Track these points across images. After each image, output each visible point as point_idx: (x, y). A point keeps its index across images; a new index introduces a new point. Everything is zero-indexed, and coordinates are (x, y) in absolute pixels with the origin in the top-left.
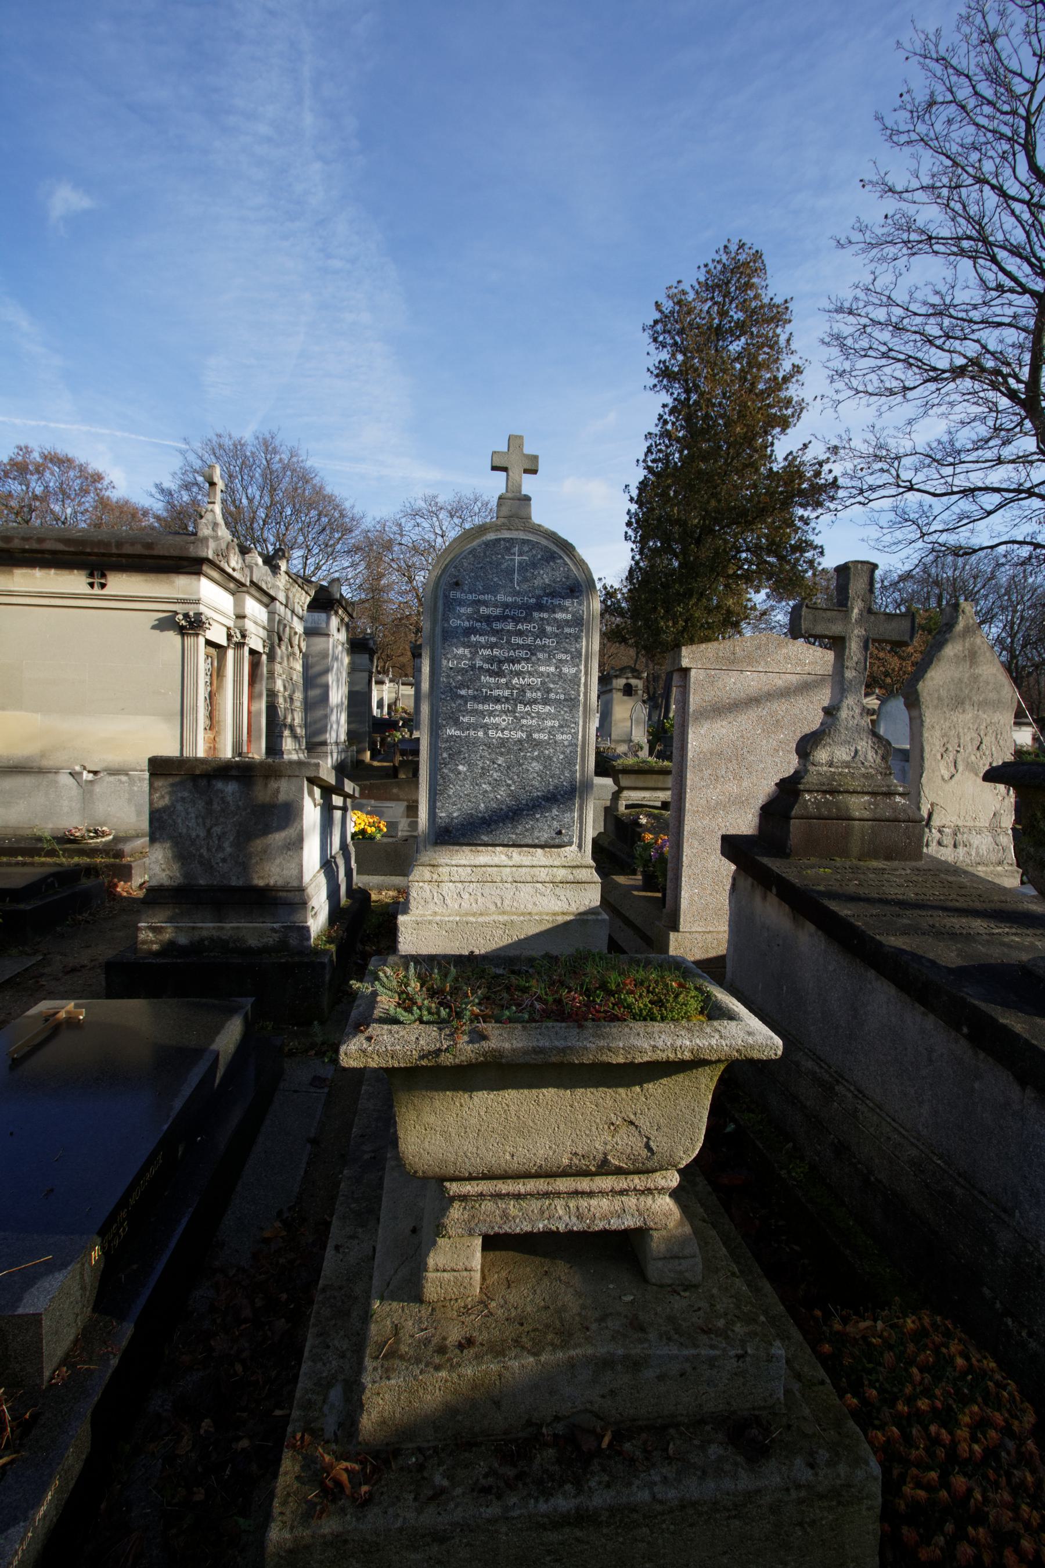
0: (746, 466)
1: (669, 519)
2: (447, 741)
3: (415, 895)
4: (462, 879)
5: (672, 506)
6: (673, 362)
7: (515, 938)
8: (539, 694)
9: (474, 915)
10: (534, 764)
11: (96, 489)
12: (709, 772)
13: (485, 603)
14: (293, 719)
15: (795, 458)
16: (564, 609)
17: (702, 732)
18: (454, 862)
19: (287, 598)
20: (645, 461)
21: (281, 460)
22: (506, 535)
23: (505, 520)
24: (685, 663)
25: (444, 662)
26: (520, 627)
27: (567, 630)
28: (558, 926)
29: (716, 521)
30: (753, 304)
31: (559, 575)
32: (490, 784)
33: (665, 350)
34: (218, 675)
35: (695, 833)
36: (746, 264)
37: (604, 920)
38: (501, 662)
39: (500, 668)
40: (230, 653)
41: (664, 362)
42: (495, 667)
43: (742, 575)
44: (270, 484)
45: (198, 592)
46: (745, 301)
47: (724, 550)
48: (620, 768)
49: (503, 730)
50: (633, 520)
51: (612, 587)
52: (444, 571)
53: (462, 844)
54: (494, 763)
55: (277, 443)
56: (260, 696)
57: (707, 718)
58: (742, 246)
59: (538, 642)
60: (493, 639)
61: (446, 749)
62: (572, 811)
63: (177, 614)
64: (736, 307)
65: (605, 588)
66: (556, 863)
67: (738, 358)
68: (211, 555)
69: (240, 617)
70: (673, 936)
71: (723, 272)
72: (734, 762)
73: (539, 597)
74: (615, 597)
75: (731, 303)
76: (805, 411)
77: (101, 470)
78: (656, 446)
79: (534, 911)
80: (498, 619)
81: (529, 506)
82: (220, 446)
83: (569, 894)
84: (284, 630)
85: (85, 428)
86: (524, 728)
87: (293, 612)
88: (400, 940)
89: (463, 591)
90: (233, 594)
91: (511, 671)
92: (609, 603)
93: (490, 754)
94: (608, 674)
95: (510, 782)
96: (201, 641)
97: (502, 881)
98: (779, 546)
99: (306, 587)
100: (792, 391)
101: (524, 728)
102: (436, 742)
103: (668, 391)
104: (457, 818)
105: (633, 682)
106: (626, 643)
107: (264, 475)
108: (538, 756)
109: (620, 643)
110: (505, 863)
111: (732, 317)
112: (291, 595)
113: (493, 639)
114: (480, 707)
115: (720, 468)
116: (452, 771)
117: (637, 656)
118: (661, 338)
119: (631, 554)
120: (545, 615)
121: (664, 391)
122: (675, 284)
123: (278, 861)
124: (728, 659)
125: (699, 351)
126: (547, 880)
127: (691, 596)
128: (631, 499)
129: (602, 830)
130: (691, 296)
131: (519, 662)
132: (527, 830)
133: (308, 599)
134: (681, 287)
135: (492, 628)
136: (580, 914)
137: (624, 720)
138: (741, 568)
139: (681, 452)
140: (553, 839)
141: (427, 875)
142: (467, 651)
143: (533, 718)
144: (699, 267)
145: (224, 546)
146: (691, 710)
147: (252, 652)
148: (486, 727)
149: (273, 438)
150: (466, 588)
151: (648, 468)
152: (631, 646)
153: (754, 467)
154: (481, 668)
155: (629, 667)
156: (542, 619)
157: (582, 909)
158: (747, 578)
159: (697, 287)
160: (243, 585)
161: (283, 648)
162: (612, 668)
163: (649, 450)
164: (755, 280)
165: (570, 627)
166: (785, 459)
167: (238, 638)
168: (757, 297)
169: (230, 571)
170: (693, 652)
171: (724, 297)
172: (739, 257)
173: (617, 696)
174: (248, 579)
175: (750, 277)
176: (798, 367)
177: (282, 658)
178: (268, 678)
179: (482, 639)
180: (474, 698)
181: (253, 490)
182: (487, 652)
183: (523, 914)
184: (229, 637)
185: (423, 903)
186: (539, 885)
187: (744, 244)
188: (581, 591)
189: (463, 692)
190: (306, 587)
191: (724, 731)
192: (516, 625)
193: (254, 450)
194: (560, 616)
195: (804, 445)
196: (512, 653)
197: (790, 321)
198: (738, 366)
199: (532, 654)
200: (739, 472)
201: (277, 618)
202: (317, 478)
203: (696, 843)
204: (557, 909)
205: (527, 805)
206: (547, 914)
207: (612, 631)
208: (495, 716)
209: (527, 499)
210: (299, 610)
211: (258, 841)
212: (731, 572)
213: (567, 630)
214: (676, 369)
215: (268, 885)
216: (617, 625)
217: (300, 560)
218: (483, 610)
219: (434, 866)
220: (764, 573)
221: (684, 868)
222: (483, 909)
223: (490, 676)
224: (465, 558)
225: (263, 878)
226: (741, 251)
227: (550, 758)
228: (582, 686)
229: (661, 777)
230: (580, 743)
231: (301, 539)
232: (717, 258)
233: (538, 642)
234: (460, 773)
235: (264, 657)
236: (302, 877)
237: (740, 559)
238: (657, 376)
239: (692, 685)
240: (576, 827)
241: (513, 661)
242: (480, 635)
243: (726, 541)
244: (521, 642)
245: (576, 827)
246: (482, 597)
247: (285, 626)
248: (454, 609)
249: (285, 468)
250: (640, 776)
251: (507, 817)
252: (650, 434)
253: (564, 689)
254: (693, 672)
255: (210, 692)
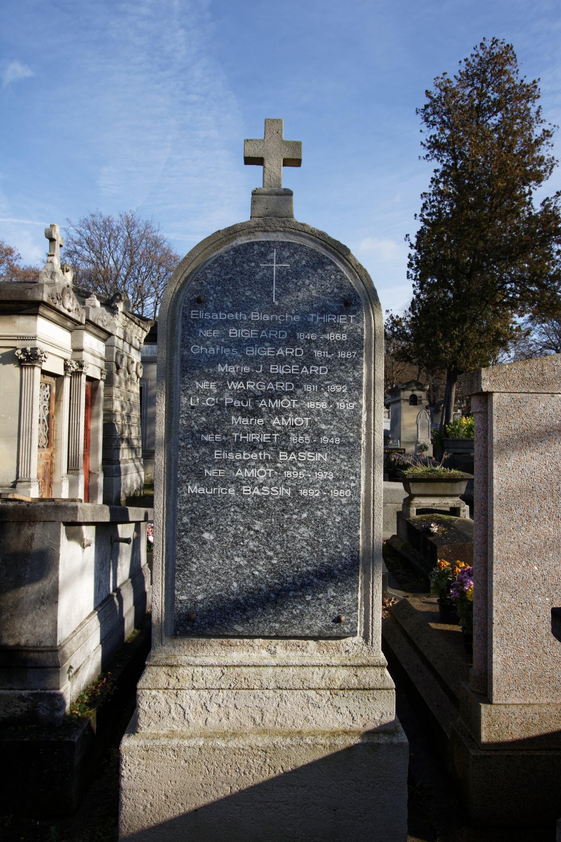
0: (508, 212)
1: (444, 260)
2: (188, 502)
3: (146, 708)
4: (209, 685)
5: (447, 248)
6: (442, 136)
7: (280, 770)
8: (307, 438)
9: (224, 736)
10: (303, 529)
11: (8, 260)
12: (520, 511)
13: (235, 323)
14: (130, 433)
15: (549, 205)
16: (337, 328)
17: (509, 465)
18: (198, 661)
19: (125, 333)
20: (421, 215)
21: (139, 232)
22: (261, 237)
23: (260, 220)
24: (486, 386)
25: (184, 400)
26: (280, 352)
27: (342, 354)
28: (338, 753)
29: (485, 259)
30: (507, 86)
31: (329, 285)
32: (245, 556)
33: (435, 127)
34: (56, 400)
35: (506, 584)
36: (499, 56)
37: (401, 744)
38: (256, 398)
39: (255, 406)
40: (67, 381)
41: (435, 136)
42: (249, 405)
43: (507, 302)
44: (130, 251)
45: (35, 330)
46: (499, 84)
47: (492, 282)
48: (411, 477)
49: (260, 486)
50: (414, 262)
51: (397, 317)
52: (183, 286)
53: (209, 636)
54: (249, 529)
55: (136, 219)
56: (98, 416)
57: (514, 449)
58: (495, 42)
59: (304, 370)
60: (247, 369)
61: (186, 512)
62: (354, 590)
63: (16, 349)
64: (493, 89)
65: (392, 318)
66: (334, 661)
67: (496, 129)
68: (45, 299)
69: (78, 350)
70: (484, 709)
71: (480, 64)
72: (549, 499)
73: (305, 314)
74: (401, 325)
75: (487, 87)
76: (555, 166)
77: (12, 247)
78: (430, 203)
79: (307, 728)
80: (251, 343)
81: (291, 201)
82: (94, 224)
83: (353, 705)
84: (121, 360)
85: (15, 221)
86: (289, 483)
87: (131, 345)
88: (124, 773)
89: (207, 310)
90: (71, 331)
91: (270, 409)
92: (396, 330)
93: (244, 517)
94: (397, 387)
95: (271, 553)
96: (37, 371)
97: (261, 688)
98: (540, 276)
99: (142, 325)
100: (544, 151)
101: (289, 483)
102: (175, 502)
103: (438, 159)
104: (202, 601)
105: (418, 393)
106: (411, 362)
107: (126, 242)
108: (308, 519)
109: (406, 362)
110: (266, 662)
111: (489, 97)
112: (128, 331)
113: (247, 369)
114: (231, 456)
115: (486, 215)
116: (195, 540)
117: (420, 372)
118: (431, 118)
119: (412, 289)
120: (313, 337)
121: (436, 159)
122: (441, 76)
123: (30, 617)
124: (536, 380)
125: (464, 126)
126: (323, 685)
127: (465, 322)
128: (411, 246)
129: (395, 533)
130: (455, 83)
131: (280, 398)
132: (295, 617)
133: (145, 334)
134: (446, 77)
135: (244, 355)
136: (368, 734)
137: (411, 425)
138: (506, 296)
139: (451, 205)
140: (329, 628)
141: (163, 680)
142: (212, 386)
143: (299, 469)
144: (460, 62)
145: (59, 291)
146: (495, 440)
147: (89, 379)
148: (238, 482)
149: (132, 215)
150: (210, 306)
151: (424, 220)
152: (415, 365)
153: (516, 213)
154: (231, 406)
155: (413, 381)
156: (309, 341)
157: (371, 726)
158: (512, 304)
159: (459, 77)
160: (80, 324)
161: (122, 375)
162: (400, 382)
163: (425, 207)
164: (507, 67)
165: (346, 350)
166: (542, 204)
167: (75, 367)
168: (509, 80)
169: (66, 312)
170: (495, 375)
171: (482, 83)
172: (493, 51)
173: (405, 406)
174: (84, 319)
175: (503, 65)
176: (548, 131)
177: (120, 383)
178: (105, 401)
179: (232, 370)
180: (223, 445)
181: (118, 254)
182: (238, 386)
183: (289, 734)
184: (66, 367)
185: (157, 719)
186: (312, 693)
187: (497, 40)
188: (359, 304)
189: (208, 438)
190: (142, 325)
191: (535, 463)
192: (276, 350)
193: (119, 225)
194: (332, 336)
195: (557, 193)
196: (270, 386)
197: (539, 97)
198: (496, 136)
199: (297, 386)
200: (503, 217)
201: (115, 350)
202: (165, 243)
203: (508, 597)
204: (336, 725)
205: (294, 583)
206: (323, 734)
207: (399, 352)
208: (249, 468)
209: (288, 193)
210: (136, 343)
211: (9, 595)
212: (498, 300)
213: (342, 354)
214: (445, 141)
215: (18, 645)
216: (403, 348)
217: (152, 305)
218: (233, 332)
219: (172, 666)
220: (527, 300)
221: (495, 626)
222: (237, 725)
223: (244, 417)
224: (210, 268)
225: (13, 636)
226: (495, 46)
227: (323, 521)
228: (363, 426)
229: (449, 485)
230: (362, 500)
231: (153, 290)
232: (475, 53)
233: (304, 370)
234: (205, 543)
235: (102, 383)
236: (56, 635)
237: (505, 289)
238: (429, 148)
239: (495, 412)
240: (360, 614)
241: (272, 396)
242: (229, 364)
243: (493, 276)
244: (282, 372)
245: (360, 614)
246: (230, 316)
247: (122, 357)
248: (196, 332)
249: (142, 237)
250: (430, 484)
251: (268, 599)
252: (425, 193)
253: (340, 430)
254: (495, 397)
255: (49, 415)
